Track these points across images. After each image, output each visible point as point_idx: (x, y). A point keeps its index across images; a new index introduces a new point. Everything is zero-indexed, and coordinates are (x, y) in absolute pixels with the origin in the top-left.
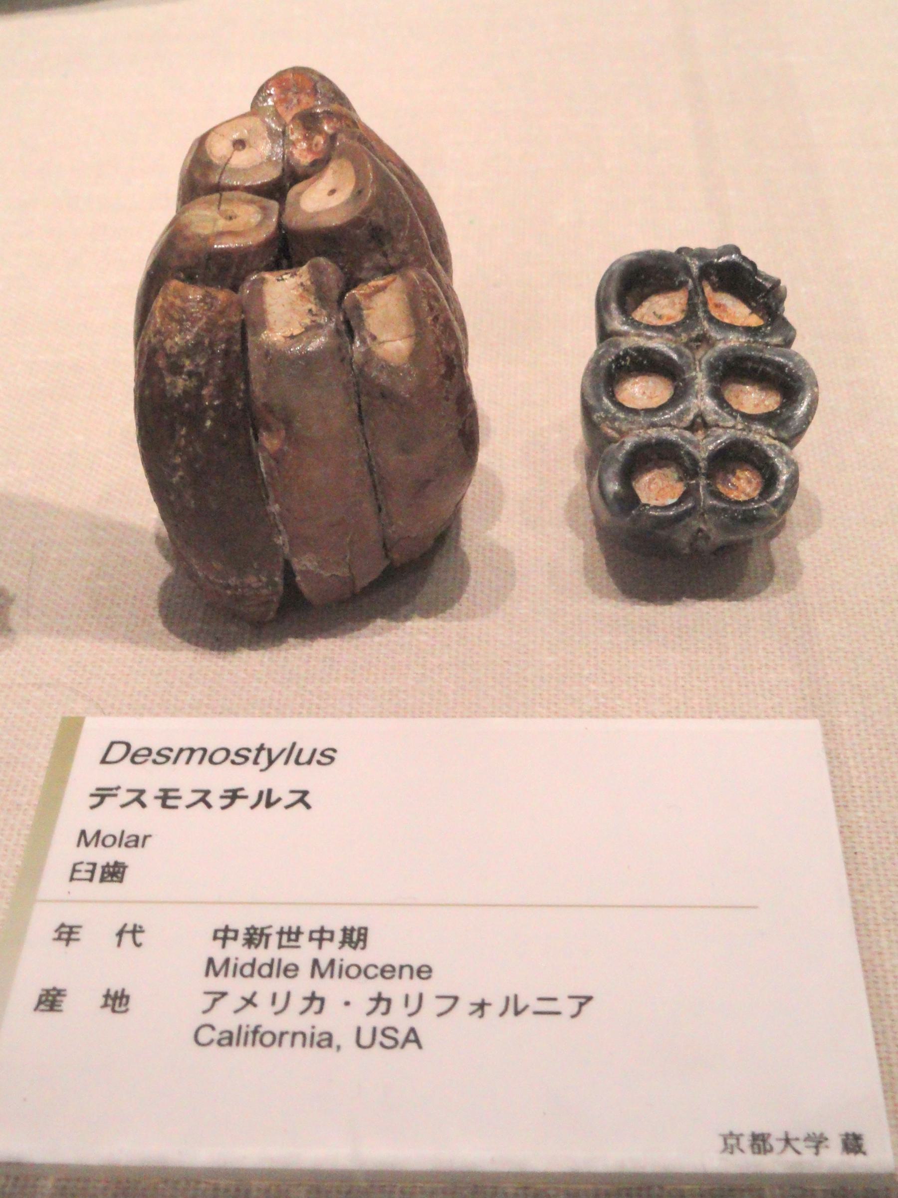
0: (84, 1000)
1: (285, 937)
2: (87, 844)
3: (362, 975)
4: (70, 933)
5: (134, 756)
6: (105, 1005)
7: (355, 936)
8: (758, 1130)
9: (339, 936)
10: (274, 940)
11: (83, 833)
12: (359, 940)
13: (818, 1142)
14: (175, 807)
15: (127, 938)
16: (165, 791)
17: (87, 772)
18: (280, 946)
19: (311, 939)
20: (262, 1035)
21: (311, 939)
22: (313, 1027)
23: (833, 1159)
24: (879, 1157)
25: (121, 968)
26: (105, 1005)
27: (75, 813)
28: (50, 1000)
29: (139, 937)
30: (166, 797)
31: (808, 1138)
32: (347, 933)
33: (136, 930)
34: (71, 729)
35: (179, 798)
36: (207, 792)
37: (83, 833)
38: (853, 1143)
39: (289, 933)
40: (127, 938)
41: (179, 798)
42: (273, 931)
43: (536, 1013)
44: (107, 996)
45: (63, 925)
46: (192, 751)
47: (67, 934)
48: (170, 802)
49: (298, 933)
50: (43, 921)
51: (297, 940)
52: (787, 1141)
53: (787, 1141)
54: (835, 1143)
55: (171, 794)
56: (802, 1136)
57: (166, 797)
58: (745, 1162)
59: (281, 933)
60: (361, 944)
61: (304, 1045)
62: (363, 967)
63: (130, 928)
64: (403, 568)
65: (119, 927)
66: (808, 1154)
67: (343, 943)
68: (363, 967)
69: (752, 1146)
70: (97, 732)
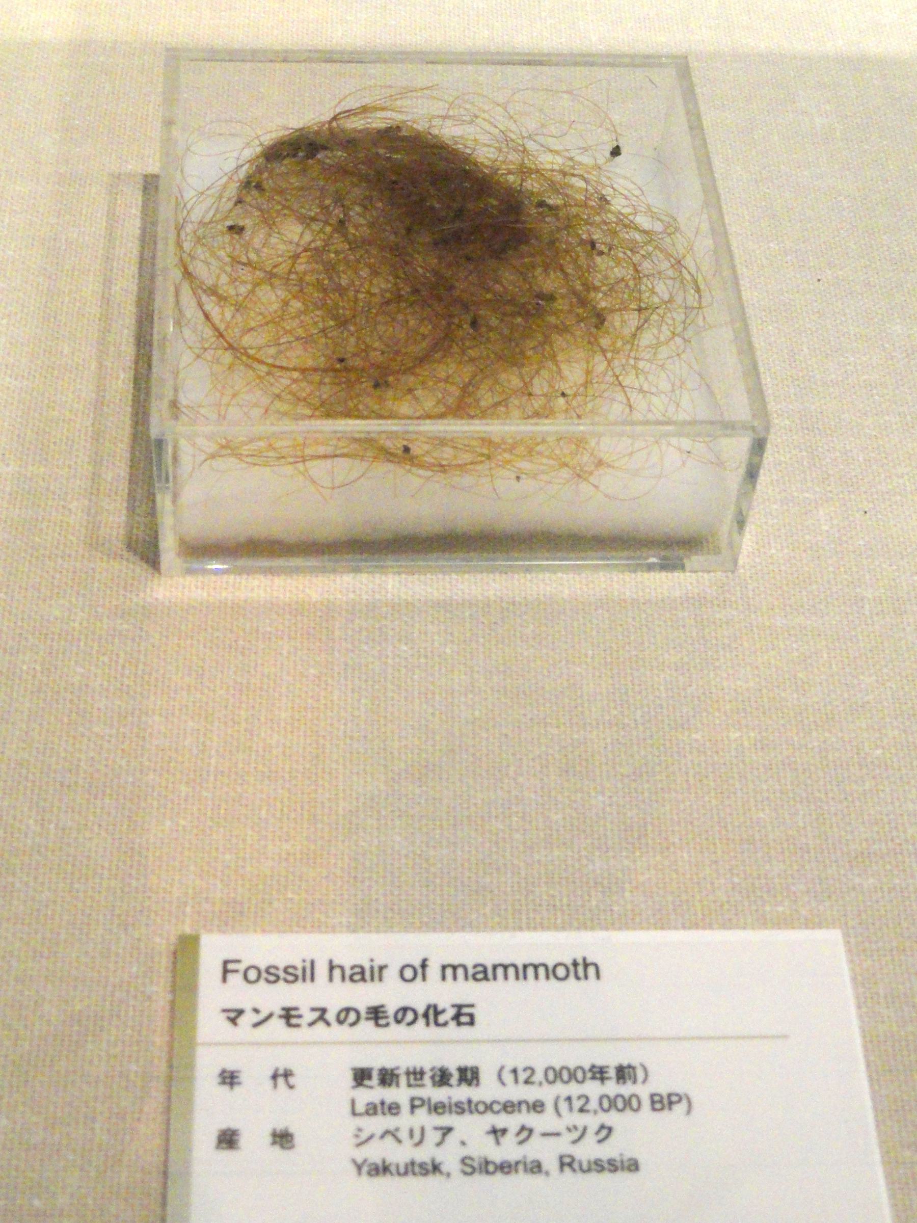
0: (256, 1139)
1: (412, 1077)
3: (551, 966)
7: (469, 1075)
9: (456, 1075)
10: (403, 1080)
12: (473, 1078)
14: (298, 1026)
15: (281, 1081)
17: (213, 995)
18: (409, 1085)
25: (280, 1109)
28: (228, 1140)
29: (292, 1080)
30: (289, 1015)
32: (462, 1071)
33: (287, 1074)
34: (186, 949)
35: (300, 1016)
36: (324, 1011)
40: (281, 1081)
41: (300, 1016)
42: (401, 1071)
43: (545, 1135)
47: (229, 1078)
48: (294, 1021)
49: (422, 1073)
50: (207, 1064)
51: (421, 1079)
55: (293, 1013)
60: (475, 1082)
61: (517, 978)
62: (551, 965)
63: (281, 1072)
65: (270, 1073)
68: (551, 965)
70: (213, 949)
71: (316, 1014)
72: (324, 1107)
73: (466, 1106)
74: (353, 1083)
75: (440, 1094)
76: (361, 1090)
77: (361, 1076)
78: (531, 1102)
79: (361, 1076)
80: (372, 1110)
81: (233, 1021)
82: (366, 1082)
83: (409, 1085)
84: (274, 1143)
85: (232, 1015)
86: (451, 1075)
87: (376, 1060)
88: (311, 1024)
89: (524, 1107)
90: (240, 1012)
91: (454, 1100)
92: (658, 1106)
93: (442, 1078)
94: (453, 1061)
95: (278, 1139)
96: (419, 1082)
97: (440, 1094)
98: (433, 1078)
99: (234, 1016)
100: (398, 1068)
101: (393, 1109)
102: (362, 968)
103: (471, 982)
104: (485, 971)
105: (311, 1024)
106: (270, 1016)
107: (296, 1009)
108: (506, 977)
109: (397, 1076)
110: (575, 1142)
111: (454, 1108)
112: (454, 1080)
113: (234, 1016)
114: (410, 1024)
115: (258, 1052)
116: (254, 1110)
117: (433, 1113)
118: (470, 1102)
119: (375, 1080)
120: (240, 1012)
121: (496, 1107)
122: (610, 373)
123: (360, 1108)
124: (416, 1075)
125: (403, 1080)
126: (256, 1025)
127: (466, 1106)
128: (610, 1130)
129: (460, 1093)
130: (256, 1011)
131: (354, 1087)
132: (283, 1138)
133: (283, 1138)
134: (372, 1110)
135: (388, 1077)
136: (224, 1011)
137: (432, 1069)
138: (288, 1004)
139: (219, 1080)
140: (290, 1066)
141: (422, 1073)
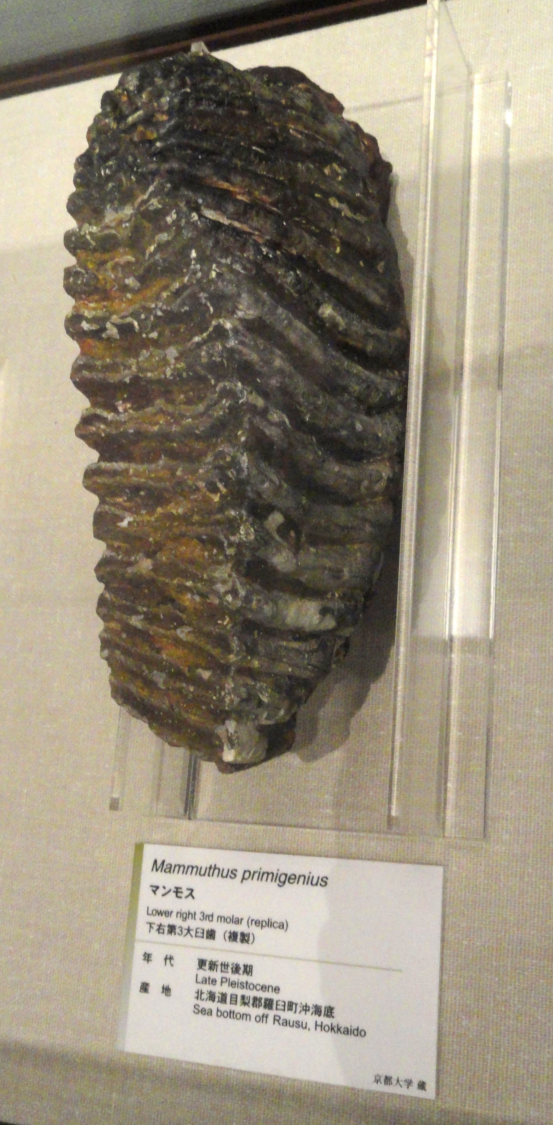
0: (155, 989)
2: (157, 870)
8: (388, 1075)
9: (242, 968)
10: (219, 967)
11: (155, 862)
13: (409, 1083)
14: (180, 897)
15: (168, 961)
16: (177, 888)
17: (149, 877)
18: (222, 971)
20: (280, 876)
22: (310, 873)
23: (414, 1092)
27: (147, 900)
29: (172, 961)
31: (406, 1081)
32: (245, 966)
33: (171, 958)
34: (139, 848)
35: (182, 892)
37: (155, 862)
40: (168, 961)
42: (219, 963)
46: (193, 868)
48: (179, 894)
50: (139, 950)
53: (398, 1081)
54: (415, 1084)
57: (177, 891)
58: (382, 1088)
59: (222, 964)
63: (168, 957)
64: (208, 932)
66: (405, 1087)
67: (244, 972)
70: (152, 853)
71: (189, 892)
72: (185, 977)
74: (198, 967)
75: (234, 978)
76: (201, 971)
77: (202, 963)
79: (202, 963)
80: (205, 981)
81: (154, 892)
84: (163, 992)
85: (154, 889)
86: (240, 968)
87: (209, 956)
88: (187, 897)
89: (270, 989)
90: (157, 888)
93: (236, 969)
94: (242, 961)
97: (234, 978)
98: (232, 969)
99: (155, 889)
100: (218, 961)
101: (214, 982)
102: (295, 876)
103: (270, 871)
105: (187, 897)
106: (170, 891)
107: (181, 888)
109: (217, 966)
112: (241, 972)
113: (155, 889)
115: (161, 945)
116: (157, 974)
117: (230, 987)
118: (247, 983)
119: (207, 967)
120: (157, 888)
123: (200, 980)
124: (225, 965)
125: (219, 967)
126: (163, 895)
129: (243, 978)
130: (164, 888)
131: (198, 969)
134: (205, 981)
135: (213, 966)
136: (151, 886)
137: (232, 964)
138: (177, 886)
139: (143, 958)
140: (172, 954)
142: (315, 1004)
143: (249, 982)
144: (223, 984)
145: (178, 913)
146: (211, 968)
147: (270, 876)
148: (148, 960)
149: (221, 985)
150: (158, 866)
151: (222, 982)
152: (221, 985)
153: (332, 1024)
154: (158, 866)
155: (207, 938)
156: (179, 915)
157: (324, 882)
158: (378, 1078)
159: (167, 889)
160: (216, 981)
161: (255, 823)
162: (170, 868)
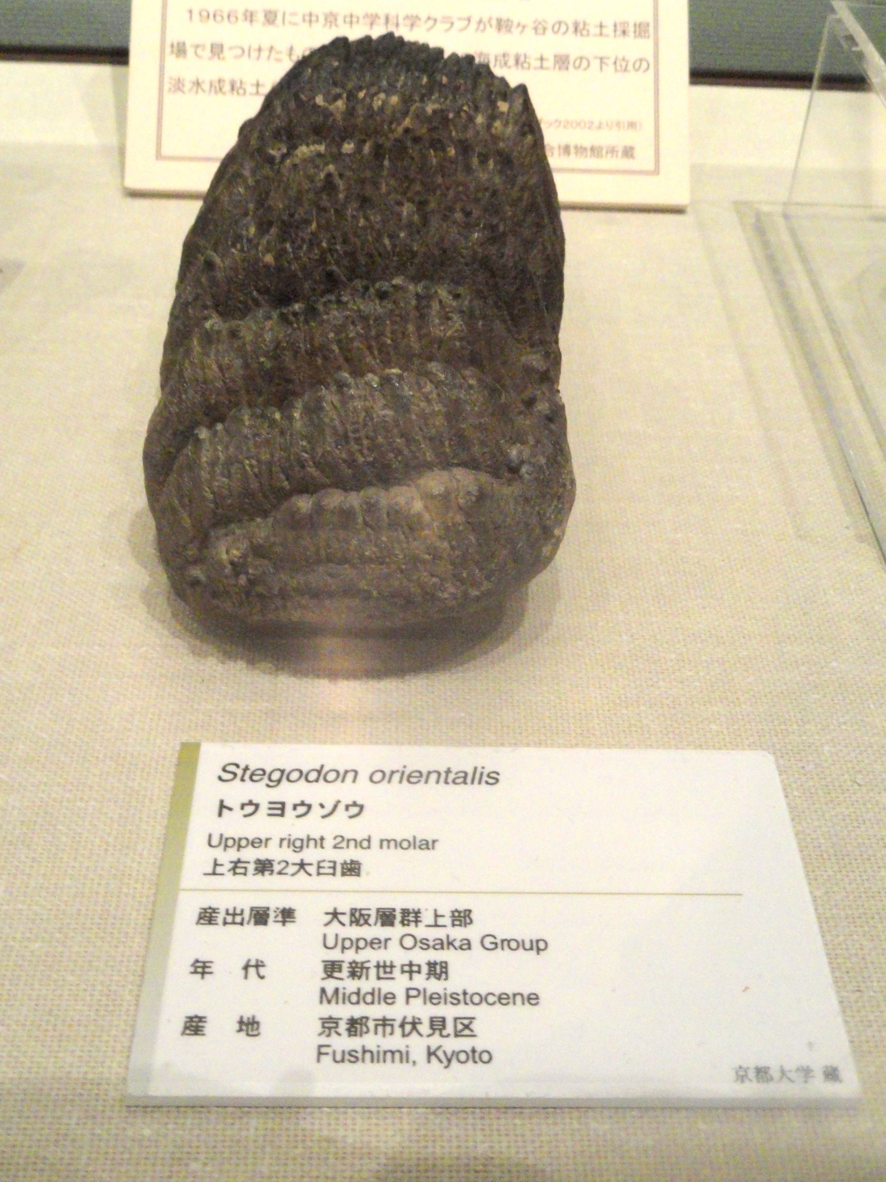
1: (381, 970)
4: (204, 967)
5: (252, 775)
6: (240, 1030)
8: (761, 1064)
10: (373, 972)
12: (442, 972)
13: (806, 1072)
15: (252, 971)
17: (207, 789)
18: (379, 978)
19: (403, 972)
21: (403, 972)
23: (820, 1088)
24: (849, 1086)
25: (251, 998)
26: (240, 1030)
28: (194, 1026)
29: (262, 971)
31: (798, 1070)
32: (405, 912)
33: (259, 965)
34: (188, 756)
38: (832, 1074)
39: (385, 966)
44: (241, 1022)
45: (197, 961)
47: (201, 968)
49: (392, 966)
51: (391, 973)
52: (783, 1072)
56: (794, 1068)
58: (751, 1090)
59: (378, 966)
60: (444, 976)
63: (253, 963)
65: (243, 964)
69: (757, 1076)
70: (213, 756)
73: (461, 998)
78: (526, 994)
82: (336, 974)
83: (379, 978)
84: (188, 1017)
91: (449, 992)
92: (444, 965)
95: (244, 1027)
96: (389, 976)
104: (427, 844)
108: (393, 1061)
110: (429, 29)
111: (449, 999)
114: (585, 69)
119: (345, 973)
121: (491, 999)
122: (542, 188)
125: (373, 972)
127: (461, 998)
128: (362, 807)
130: (322, 806)
132: (249, 1026)
133: (249, 1026)
141: (392, 966)
142: (281, 907)
143: (479, 1049)
144: (411, 1000)
145: (282, 840)
146: (353, 974)
147: (397, 1055)
148: (203, 973)
149: (407, 1002)
150: (231, 772)
151: (408, 997)
152: (407, 1002)
153: (448, 936)
154: (231, 772)
155: (343, 874)
156: (285, 843)
157: (493, 778)
158: (742, 1073)
159: (329, 808)
160: (394, 997)
161: (362, 1107)
162: (465, 777)
